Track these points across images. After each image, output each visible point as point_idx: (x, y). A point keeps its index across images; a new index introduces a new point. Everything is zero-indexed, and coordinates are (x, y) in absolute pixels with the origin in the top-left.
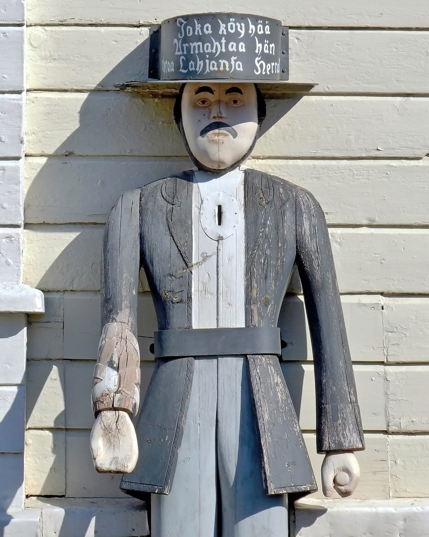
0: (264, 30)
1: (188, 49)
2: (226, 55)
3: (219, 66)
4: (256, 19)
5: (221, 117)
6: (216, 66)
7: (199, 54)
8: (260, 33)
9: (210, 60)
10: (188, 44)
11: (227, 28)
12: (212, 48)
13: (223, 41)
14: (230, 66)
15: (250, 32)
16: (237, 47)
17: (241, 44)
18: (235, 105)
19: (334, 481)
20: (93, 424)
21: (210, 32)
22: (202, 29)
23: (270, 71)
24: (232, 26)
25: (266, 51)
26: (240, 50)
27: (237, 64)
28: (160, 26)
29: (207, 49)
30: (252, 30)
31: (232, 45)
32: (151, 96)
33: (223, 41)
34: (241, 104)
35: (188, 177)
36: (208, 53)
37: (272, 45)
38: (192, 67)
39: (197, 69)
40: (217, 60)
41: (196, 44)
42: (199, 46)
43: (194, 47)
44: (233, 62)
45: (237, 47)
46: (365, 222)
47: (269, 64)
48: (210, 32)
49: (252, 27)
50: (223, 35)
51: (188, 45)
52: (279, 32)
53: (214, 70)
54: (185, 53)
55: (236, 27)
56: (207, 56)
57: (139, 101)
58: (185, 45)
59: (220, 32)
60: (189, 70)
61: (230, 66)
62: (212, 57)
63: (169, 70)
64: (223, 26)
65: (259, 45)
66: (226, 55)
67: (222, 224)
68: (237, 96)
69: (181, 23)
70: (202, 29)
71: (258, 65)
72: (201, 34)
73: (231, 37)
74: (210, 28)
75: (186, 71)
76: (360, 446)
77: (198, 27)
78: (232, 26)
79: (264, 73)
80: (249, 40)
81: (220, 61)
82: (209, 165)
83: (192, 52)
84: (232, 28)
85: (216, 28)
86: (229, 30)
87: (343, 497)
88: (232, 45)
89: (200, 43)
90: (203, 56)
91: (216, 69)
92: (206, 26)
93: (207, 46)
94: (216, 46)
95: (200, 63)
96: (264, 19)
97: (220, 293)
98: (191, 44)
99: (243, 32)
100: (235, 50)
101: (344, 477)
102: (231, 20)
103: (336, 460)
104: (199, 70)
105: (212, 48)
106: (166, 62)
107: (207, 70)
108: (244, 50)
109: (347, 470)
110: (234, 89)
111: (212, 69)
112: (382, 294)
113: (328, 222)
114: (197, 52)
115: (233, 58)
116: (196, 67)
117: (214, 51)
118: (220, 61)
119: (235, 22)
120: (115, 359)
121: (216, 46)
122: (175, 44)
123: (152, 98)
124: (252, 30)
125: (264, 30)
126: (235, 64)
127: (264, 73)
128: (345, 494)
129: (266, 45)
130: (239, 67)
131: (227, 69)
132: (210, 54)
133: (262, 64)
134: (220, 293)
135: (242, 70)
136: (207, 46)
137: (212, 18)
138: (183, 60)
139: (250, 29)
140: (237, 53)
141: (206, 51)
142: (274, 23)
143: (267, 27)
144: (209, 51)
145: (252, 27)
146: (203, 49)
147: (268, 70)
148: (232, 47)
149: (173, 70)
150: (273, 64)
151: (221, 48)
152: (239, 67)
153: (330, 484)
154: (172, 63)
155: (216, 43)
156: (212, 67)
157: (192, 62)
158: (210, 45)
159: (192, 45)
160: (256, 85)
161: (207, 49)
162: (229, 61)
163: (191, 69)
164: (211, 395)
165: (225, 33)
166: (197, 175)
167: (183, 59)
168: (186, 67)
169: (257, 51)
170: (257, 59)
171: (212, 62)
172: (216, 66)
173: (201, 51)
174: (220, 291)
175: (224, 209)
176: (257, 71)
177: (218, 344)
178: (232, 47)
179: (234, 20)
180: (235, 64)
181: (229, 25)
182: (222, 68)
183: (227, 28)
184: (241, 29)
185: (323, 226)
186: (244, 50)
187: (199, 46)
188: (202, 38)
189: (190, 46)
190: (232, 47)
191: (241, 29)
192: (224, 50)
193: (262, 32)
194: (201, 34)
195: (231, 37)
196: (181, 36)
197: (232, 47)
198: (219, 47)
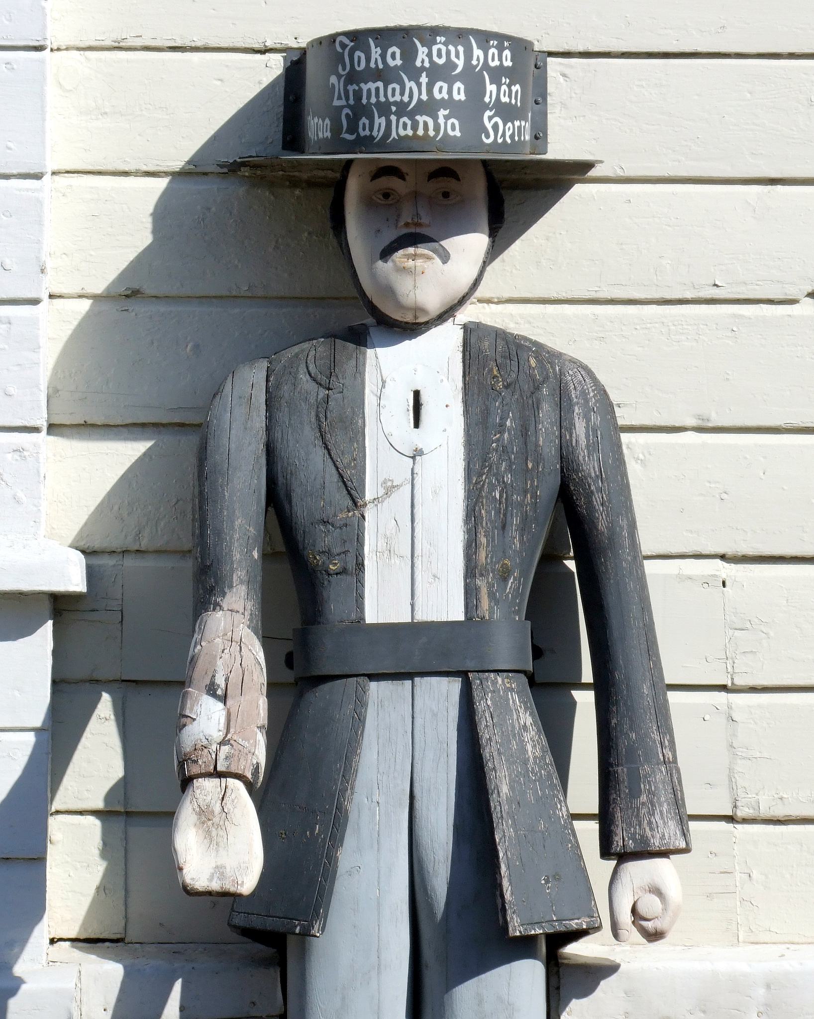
0: (500, 59)
1: (358, 95)
2: (430, 107)
3: (415, 127)
4: (485, 38)
6: (409, 127)
7: (378, 102)
9: (399, 115)
10: (358, 85)
11: (430, 55)
12: (402, 94)
13: (424, 79)
14: (437, 128)
15: (474, 62)
16: (450, 92)
17: (458, 85)
19: (634, 911)
21: (398, 62)
22: (383, 56)
23: (512, 137)
24: (439, 51)
25: (505, 99)
26: (456, 97)
27: (450, 122)
28: (303, 52)
29: (393, 95)
30: (478, 59)
31: (441, 88)
32: (288, 183)
33: (424, 79)
35: (359, 338)
36: (395, 103)
37: (516, 88)
40: (412, 115)
41: (372, 86)
43: (369, 91)
44: (441, 121)
45: (450, 92)
46: (691, 422)
47: (509, 124)
49: (478, 53)
50: (423, 69)
53: (407, 136)
54: (352, 102)
55: (448, 53)
56: (394, 109)
58: (351, 88)
59: (418, 64)
60: (358, 134)
61: (437, 128)
62: (402, 109)
63: (321, 135)
64: (422, 51)
65: (491, 88)
66: (430, 107)
69: (343, 46)
70: (383, 56)
71: (489, 126)
72: (381, 66)
73: (437, 73)
74: (398, 55)
75: (351, 137)
76: (683, 845)
77: (376, 52)
78: (439, 51)
79: (500, 141)
80: (473, 80)
81: (418, 117)
83: (364, 101)
84: (439, 55)
85: (409, 55)
86: (435, 58)
87: (650, 941)
88: (441, 88)
89: (380, 84)
90: (384, 109)
91: (410, 132)
92: (390, 51)
93: (394, 90)
94: (411, 89)
95: (380, 122)
96: (501, 38)
98: (362, 85)
99: (460, 63)
100: (446, 97)
101: (650, 905)
102: (438, 39)
103: (638, 872)
104: (378, 134)
105: (402, 94)
106: (316, 120)
107: (394, 135)
109: (657, 891)
110: (445, 172)
111: (402, 133)
112: (723, 557)
114: (373, 100)
115: (442, 113)
117: (406, 99)
118: (418, 117)
119: (446, 44)
121: (411, 89)
122: (333, 85)
124: (478, 59)
125: (500, 59)
126: (446, 124)
128: (654, 936)
129: (504, 87)
130: (453, 129)
131: (431, 133)
136: (394, 90)
137: (402, 36)
138: (347, 115)
139: (475, 58)
140: (448, 103)
141: (391, 100)
143: (507, 53)
144: (397, 98)
145: (478, 53)
146: (386, 95)
147: (508, 134)
148: (440, 91)
150: (517, 123)
151: (420, 93)
152: (453, 129)
153: (625, 917)
154: (327, 121)
155: (410, 84)
156: (402, 129)
158: (397, 87)
159: (365, 87)
160: (485, 163)
162: (435, 118)
163: (362, 134)
165: (427, 64)
168: (353, 129)
169: (487, 99)
170: (488, 113)
171: (402, 120)
172: (409, 127)
173: (382, 99)
174: (418, 552)
175: (424, 398)
176: (488, 137)
177: (415, 652)
179: (443, 39)
180: (446, 124)
181: (435, 48)
182: (420, 132)
183: (430, 55)
184: (457, 56)
185: (610, 431)
187: (377, 89)
188: (384, 75)
189: (361, 90)
190: (440, 91)
191: (457, 56)
192: (424, 97)
193: (496, 63)
194: (381, 66)
196: (344, 69)
198: (415, 91)
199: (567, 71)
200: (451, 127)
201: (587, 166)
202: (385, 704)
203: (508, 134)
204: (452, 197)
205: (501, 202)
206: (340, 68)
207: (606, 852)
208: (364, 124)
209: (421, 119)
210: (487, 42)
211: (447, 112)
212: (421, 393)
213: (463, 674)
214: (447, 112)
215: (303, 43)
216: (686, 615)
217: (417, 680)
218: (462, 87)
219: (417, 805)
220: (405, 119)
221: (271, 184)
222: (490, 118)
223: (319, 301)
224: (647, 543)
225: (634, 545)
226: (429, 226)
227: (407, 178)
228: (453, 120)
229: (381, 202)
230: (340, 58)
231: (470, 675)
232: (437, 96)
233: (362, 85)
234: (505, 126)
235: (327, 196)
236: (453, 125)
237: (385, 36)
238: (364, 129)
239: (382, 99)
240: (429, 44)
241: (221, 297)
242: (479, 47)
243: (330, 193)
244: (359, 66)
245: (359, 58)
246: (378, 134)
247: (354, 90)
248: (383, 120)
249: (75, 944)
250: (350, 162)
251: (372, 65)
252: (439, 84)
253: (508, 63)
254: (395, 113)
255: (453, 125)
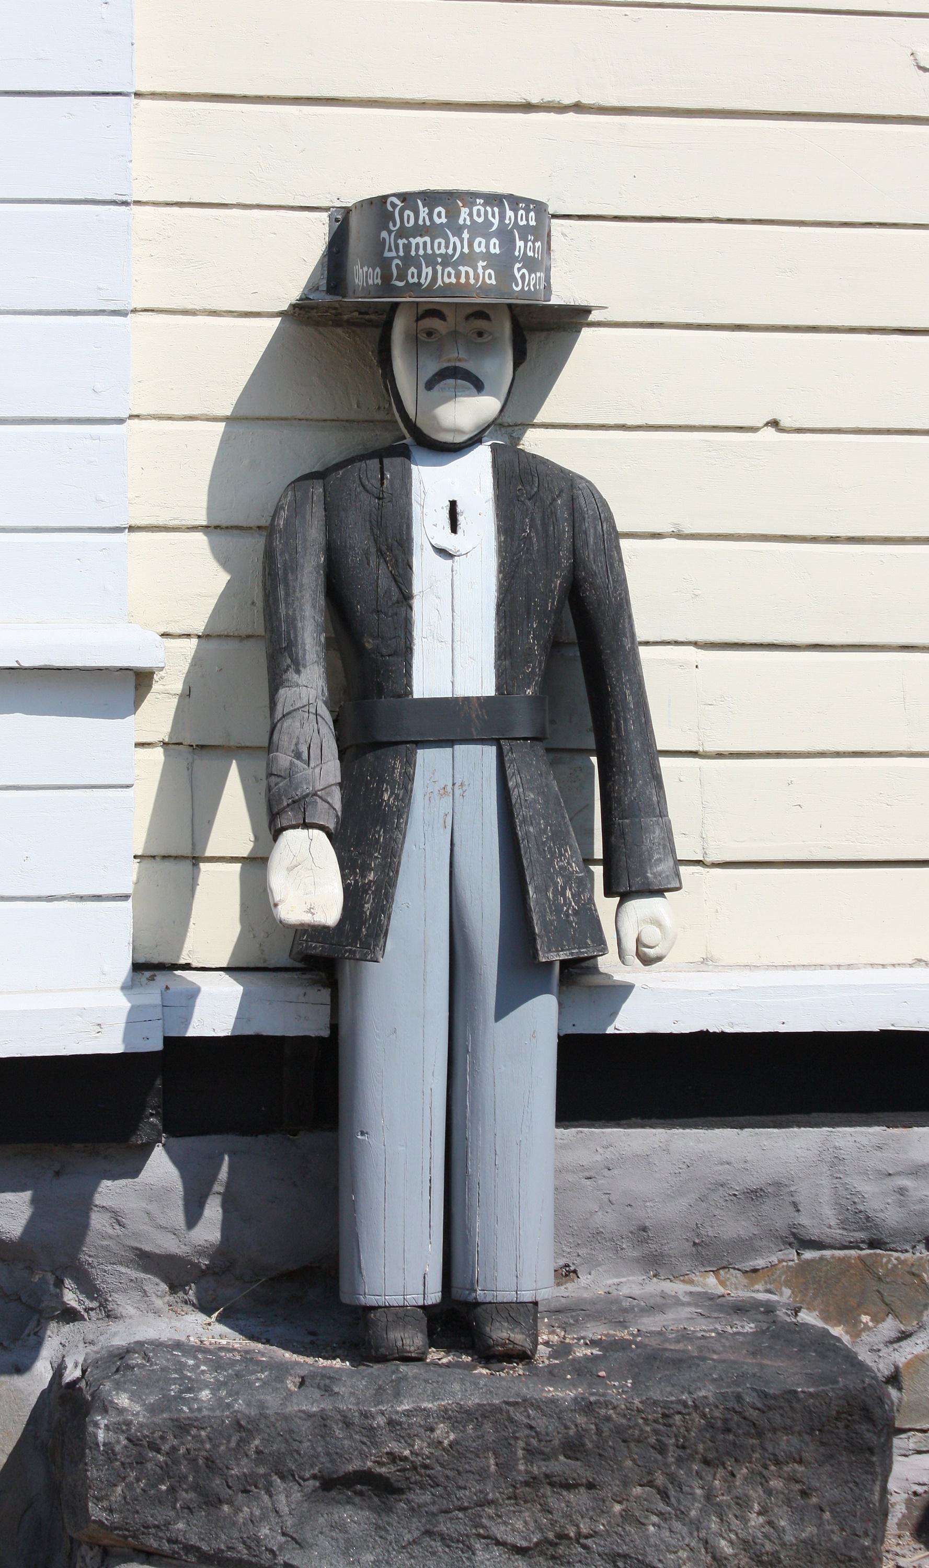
0: (527, 220)
1: (407, 247)
2: (469, 259)
3: (458, 276)
4: (515, 201)
5: (460, 360)
6: (453, 276)
7: (426, 255)
8: (521, 223)
9: (445, 264)
10: (407, 239)
11: (470, 215)
12: (447, 247)
13: (466, 235)
14: (476, 277)
15: (507, 222)
16: (487, 246)
17: (494, 240)
18: (480, 340)
19: (638, 941)
20: (271, 849)
21: (444, 220)
22: (430, 215)
23: (535, 285)
24: (479, 210)
25: (530, 254)
26: (492, 251)
27: (487, 272)
28: (347, 211)
29: (439, 248)
30: (510, 219)
31: (480, 243)
32: (330, 323)
33: (466, 235)
34: (490, 338)
35: (404, 453)
36: (441, 255)
37: (538, 244)
38: (413, 277)
39: (423, 281)
40: (455, 265)
41: (420, 240)
42: (425, 243)
43: (417, 244)
44: (480, 271)
45: (487, 246)
46: (668, 529)
47: (533, 275)
48: (444, 220)
49: (510, 213)
50: (465, 226)
51: (406, 242)
52: (535, 219)
53: (451, 283)
54: (401, 253)
55: (486, 212)
56: (439, 260)
57: (310, 330)
58: (401, 242)
59: (461, 222)
60: (407, 281)
61: (476, 277)
62: (447, 261)
63: (370, 282)
64: (464, 212)
65: (520, 244)
66: (469, 259)
67: (460, 531)
68: (481, 324)
69: (394, 205)
70: (430, 215)
71: (518, 276)
72: (428, 223)
73: (479, 230)
74: (443, 214)
75: (401, 284)
76: (678, 885)
77: (423, 211)
78: (479, 210)
79: (526, 289)
80: (506, 236)
81: (460, 268)
82: (460, 439)
83: (413, 253)
84: (479, 215)
85: (453, 215)
86: (475, 218)
87: (645, 965)
88: (480, 243)
89: (427, 239)
90: (431, 260)
91: (453, 280)
92: (436, 210)
93: (440, 244)
94: (454, 243)
95: (427, 271)
96: (528, 201)
97: (454, 644)
98: (411, 239)
99: (496, 222)
100: (484, 251)
101: (651, 935)
102: (478, 201)
103: (639, 907)
104: (425, 281)
105: (447, 247)
106: (365, 269)
107: (440, 282)
108: (497, 251)
109: (657, 923)
110: (480, 313)
111: (447, 280)
112: (695, 644)
113: (619, 529)
114: (421, 252)
115: (481, 264)
116: (419, 277)
117: (450, 251)
118: (460, 268)
119: (484, 205)
120: (304, 749)
121: (454, 243)
122: (384, 239)
123: (332, 326)
124: (510, 219)
125: (527, 220)
126: (484, 273)
127: (526, 289)
128: (647, 961)
129: (530, 244)
130: (490, 278)
131: (472, 281)
132: (445, 257)
133: (523, 274)
134: (454, 644)
135: (494, 283)
136: (440, 244)
137: (446, 199)
138: (397, 265)
139: (507, 218)
140: (487, 256)
141: (438, 252)
142: (539, 207)
143: (532, 214)
144: (443, 251)
145: (510, 213)
146: (432, 248)
147: (532, 283)
148: (480, 245)
149: (379, 281)
150: (538, 274)
151: (462, 247)
152: (490, 278)
153: (630, 946)
154: (378, 270)
155: (453, 239)
156: (447, 277)
157: (413, 269)
158: (443, 242)
159: (414, 241)
160: (510, 306)
161: (439, 248)
162: (475, 269)
163: (411, 281)
164: (452, 803)
165: (468, 223)
166: (416, 452)
167: (397, 265)
168: (402, 276)
169: (517, 253)
170: (517, 265)
171: (446, 270)
172: (453, 276)
173: (429, 251)
174: (457, 638)
175: (459, 508)
176: (517, 285)
177: (452, 722)
178: (479, 246)
179: (482, 201)
180: (484, 273)
181: (475, 209)
182: (463, 280)
183: (470, 215)
184: (493, 216)
185: (611, 538)
186: (497, 251)
187: (425, 243)
188: (432, 231)
189: (410, 243)
190: (480, 245)
191: (493, 216)
192: (466, 250)
193: (524, 222)
194: (428, 223)
195: (479, 230)
196: (395, 225)
197: (479, 246)
198: (458, 245)
199: (566, 231)
200: (489, 277)
201: (587, 311)
202: (431, 764)
203: (532, 283)
204: (485, 336)
205: (524, 342)
206: (391, 224)
207: (608, 893)
208: (413, 273)
209: (463, 269)
210: (517, 204)
211: (485, 264)
212: (458, 503)
213: (497, 742)
214: (485, 264)
215: (349, 201)
216: (676, 694)
217: (457, 747)
218: (497, 242)
219: (456, 849)
220: (450, 269)
221: (317, 324)
222: (519, 269)
223: (349, 423)
224: (641, 633)
225: (633, 635)
226: (466, 361)
227: (448, 319)
228: (490, 271)
229: (420, 341)
230: (391, 216)
231: (501, 741)
232: (477, 249)
233: (411, 239)
234: (530, 276)
235: (398, 333)
236: (490, 274)
237: (432, 198)
238: (413, 277)
239: (429, 251)
240: (471, 205)
241: (286, 419)
242: (510, 209)
243: (377, 333)
244: (408, 222)
245: (409, 216)
246: (425, 281)
247: (404, 244)
248: (430, 270)
249: (235, 974)
250: (397, 304)
251: (421, 222)
252: (478, 240)
253: (533, 223)
254: (441, 264)
255: (490, 274)
